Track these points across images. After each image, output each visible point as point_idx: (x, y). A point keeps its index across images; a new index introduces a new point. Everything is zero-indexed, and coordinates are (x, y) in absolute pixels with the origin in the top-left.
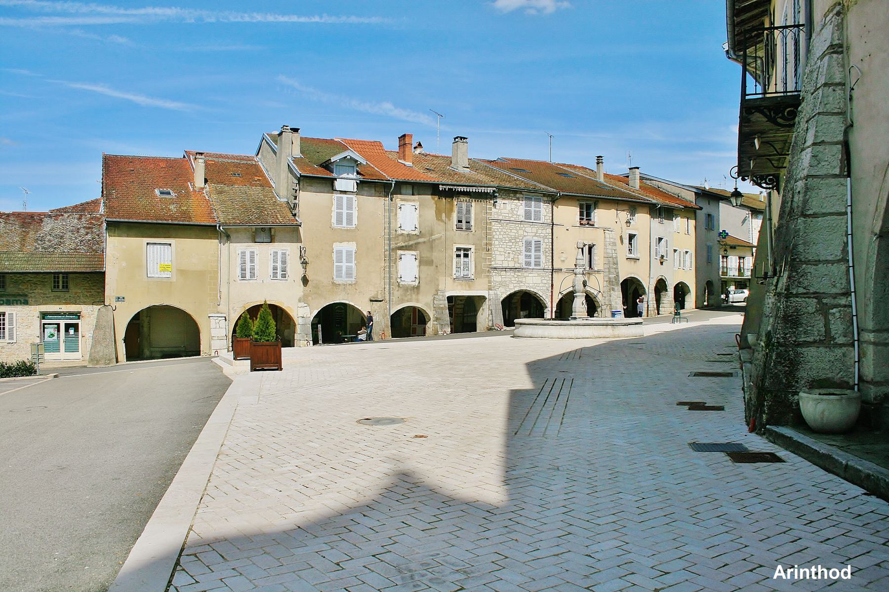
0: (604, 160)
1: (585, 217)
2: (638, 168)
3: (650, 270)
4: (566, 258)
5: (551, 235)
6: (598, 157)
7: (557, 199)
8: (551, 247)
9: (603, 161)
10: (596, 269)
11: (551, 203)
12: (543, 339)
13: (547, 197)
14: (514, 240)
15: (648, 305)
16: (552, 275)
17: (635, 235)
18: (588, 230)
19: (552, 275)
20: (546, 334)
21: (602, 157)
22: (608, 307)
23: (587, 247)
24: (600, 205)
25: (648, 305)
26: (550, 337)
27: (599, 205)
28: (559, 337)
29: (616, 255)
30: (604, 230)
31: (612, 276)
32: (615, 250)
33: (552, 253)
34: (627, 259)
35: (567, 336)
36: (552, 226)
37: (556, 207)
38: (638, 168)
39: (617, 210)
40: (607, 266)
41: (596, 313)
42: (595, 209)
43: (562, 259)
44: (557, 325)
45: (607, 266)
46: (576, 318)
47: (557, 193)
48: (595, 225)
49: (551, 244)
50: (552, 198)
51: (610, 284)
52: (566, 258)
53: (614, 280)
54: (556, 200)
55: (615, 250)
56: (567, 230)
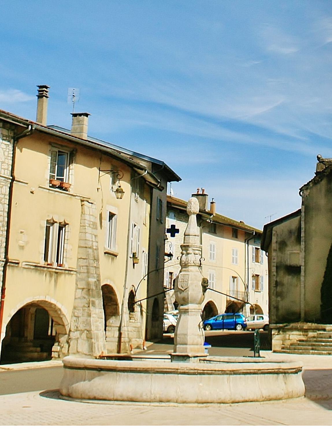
0: (50, 92)
1: (56, 175)
2: (87, 115)
3: (126, 275)
4: (27, 243)
5: (8, 197)
6: (40, 87)
7: (25, 136)
8: (6, 219)
9: (48, 94)
10: (66, 267)
11: (12, 141)
12: (163, 404)
13: (8, 130)
14: (69, 192)
15: (120, 334)
16: (4, 271)
17: (115, 214)
18: (59, 196)
19: (4, 271)
20: (172, 394)
21: (47, 88)
22: (84, 335)
23: (57, 226)
24: (79, 157)
25: (120, 334)
26: (180, 399)
27: (77, 156)
28: (200, 399)
29: (96, 243)
30: (82, 201)
31: (92, 280)
32: (96, 236)
33: (8, 231)
34: (105, 253)
35: (214, 397)
36: (11, 184)
37: (19, 150)
38: (87, 115)
39: (100, 171)
40: (83, 263)
41: (56, 344)
42: (71, 162)
43: (21, 243)
44: (194, 374)
45: (83, 263)
46: (188, 357)
47: (28, 125)
48: (70, 189)
49: (6, 215)
50: (14, 134)
51: (89, 294)
52: (27, 243)
53: (94, 288)
54: (22, 137)
55: (96, 236)
56: (32, 192)
